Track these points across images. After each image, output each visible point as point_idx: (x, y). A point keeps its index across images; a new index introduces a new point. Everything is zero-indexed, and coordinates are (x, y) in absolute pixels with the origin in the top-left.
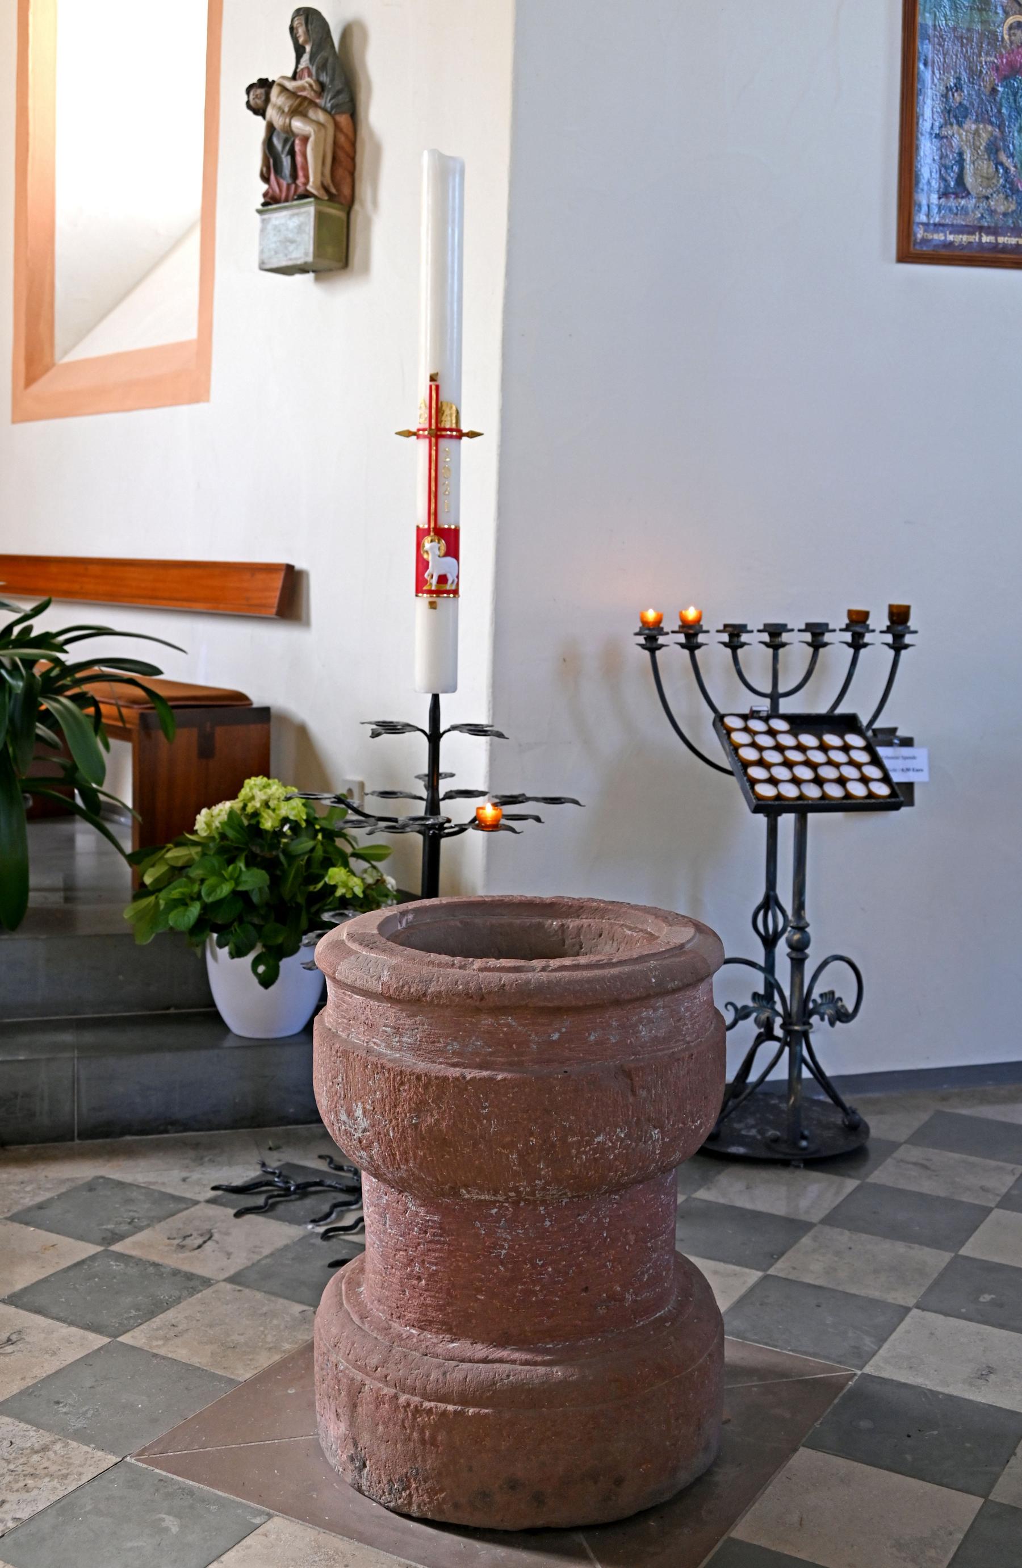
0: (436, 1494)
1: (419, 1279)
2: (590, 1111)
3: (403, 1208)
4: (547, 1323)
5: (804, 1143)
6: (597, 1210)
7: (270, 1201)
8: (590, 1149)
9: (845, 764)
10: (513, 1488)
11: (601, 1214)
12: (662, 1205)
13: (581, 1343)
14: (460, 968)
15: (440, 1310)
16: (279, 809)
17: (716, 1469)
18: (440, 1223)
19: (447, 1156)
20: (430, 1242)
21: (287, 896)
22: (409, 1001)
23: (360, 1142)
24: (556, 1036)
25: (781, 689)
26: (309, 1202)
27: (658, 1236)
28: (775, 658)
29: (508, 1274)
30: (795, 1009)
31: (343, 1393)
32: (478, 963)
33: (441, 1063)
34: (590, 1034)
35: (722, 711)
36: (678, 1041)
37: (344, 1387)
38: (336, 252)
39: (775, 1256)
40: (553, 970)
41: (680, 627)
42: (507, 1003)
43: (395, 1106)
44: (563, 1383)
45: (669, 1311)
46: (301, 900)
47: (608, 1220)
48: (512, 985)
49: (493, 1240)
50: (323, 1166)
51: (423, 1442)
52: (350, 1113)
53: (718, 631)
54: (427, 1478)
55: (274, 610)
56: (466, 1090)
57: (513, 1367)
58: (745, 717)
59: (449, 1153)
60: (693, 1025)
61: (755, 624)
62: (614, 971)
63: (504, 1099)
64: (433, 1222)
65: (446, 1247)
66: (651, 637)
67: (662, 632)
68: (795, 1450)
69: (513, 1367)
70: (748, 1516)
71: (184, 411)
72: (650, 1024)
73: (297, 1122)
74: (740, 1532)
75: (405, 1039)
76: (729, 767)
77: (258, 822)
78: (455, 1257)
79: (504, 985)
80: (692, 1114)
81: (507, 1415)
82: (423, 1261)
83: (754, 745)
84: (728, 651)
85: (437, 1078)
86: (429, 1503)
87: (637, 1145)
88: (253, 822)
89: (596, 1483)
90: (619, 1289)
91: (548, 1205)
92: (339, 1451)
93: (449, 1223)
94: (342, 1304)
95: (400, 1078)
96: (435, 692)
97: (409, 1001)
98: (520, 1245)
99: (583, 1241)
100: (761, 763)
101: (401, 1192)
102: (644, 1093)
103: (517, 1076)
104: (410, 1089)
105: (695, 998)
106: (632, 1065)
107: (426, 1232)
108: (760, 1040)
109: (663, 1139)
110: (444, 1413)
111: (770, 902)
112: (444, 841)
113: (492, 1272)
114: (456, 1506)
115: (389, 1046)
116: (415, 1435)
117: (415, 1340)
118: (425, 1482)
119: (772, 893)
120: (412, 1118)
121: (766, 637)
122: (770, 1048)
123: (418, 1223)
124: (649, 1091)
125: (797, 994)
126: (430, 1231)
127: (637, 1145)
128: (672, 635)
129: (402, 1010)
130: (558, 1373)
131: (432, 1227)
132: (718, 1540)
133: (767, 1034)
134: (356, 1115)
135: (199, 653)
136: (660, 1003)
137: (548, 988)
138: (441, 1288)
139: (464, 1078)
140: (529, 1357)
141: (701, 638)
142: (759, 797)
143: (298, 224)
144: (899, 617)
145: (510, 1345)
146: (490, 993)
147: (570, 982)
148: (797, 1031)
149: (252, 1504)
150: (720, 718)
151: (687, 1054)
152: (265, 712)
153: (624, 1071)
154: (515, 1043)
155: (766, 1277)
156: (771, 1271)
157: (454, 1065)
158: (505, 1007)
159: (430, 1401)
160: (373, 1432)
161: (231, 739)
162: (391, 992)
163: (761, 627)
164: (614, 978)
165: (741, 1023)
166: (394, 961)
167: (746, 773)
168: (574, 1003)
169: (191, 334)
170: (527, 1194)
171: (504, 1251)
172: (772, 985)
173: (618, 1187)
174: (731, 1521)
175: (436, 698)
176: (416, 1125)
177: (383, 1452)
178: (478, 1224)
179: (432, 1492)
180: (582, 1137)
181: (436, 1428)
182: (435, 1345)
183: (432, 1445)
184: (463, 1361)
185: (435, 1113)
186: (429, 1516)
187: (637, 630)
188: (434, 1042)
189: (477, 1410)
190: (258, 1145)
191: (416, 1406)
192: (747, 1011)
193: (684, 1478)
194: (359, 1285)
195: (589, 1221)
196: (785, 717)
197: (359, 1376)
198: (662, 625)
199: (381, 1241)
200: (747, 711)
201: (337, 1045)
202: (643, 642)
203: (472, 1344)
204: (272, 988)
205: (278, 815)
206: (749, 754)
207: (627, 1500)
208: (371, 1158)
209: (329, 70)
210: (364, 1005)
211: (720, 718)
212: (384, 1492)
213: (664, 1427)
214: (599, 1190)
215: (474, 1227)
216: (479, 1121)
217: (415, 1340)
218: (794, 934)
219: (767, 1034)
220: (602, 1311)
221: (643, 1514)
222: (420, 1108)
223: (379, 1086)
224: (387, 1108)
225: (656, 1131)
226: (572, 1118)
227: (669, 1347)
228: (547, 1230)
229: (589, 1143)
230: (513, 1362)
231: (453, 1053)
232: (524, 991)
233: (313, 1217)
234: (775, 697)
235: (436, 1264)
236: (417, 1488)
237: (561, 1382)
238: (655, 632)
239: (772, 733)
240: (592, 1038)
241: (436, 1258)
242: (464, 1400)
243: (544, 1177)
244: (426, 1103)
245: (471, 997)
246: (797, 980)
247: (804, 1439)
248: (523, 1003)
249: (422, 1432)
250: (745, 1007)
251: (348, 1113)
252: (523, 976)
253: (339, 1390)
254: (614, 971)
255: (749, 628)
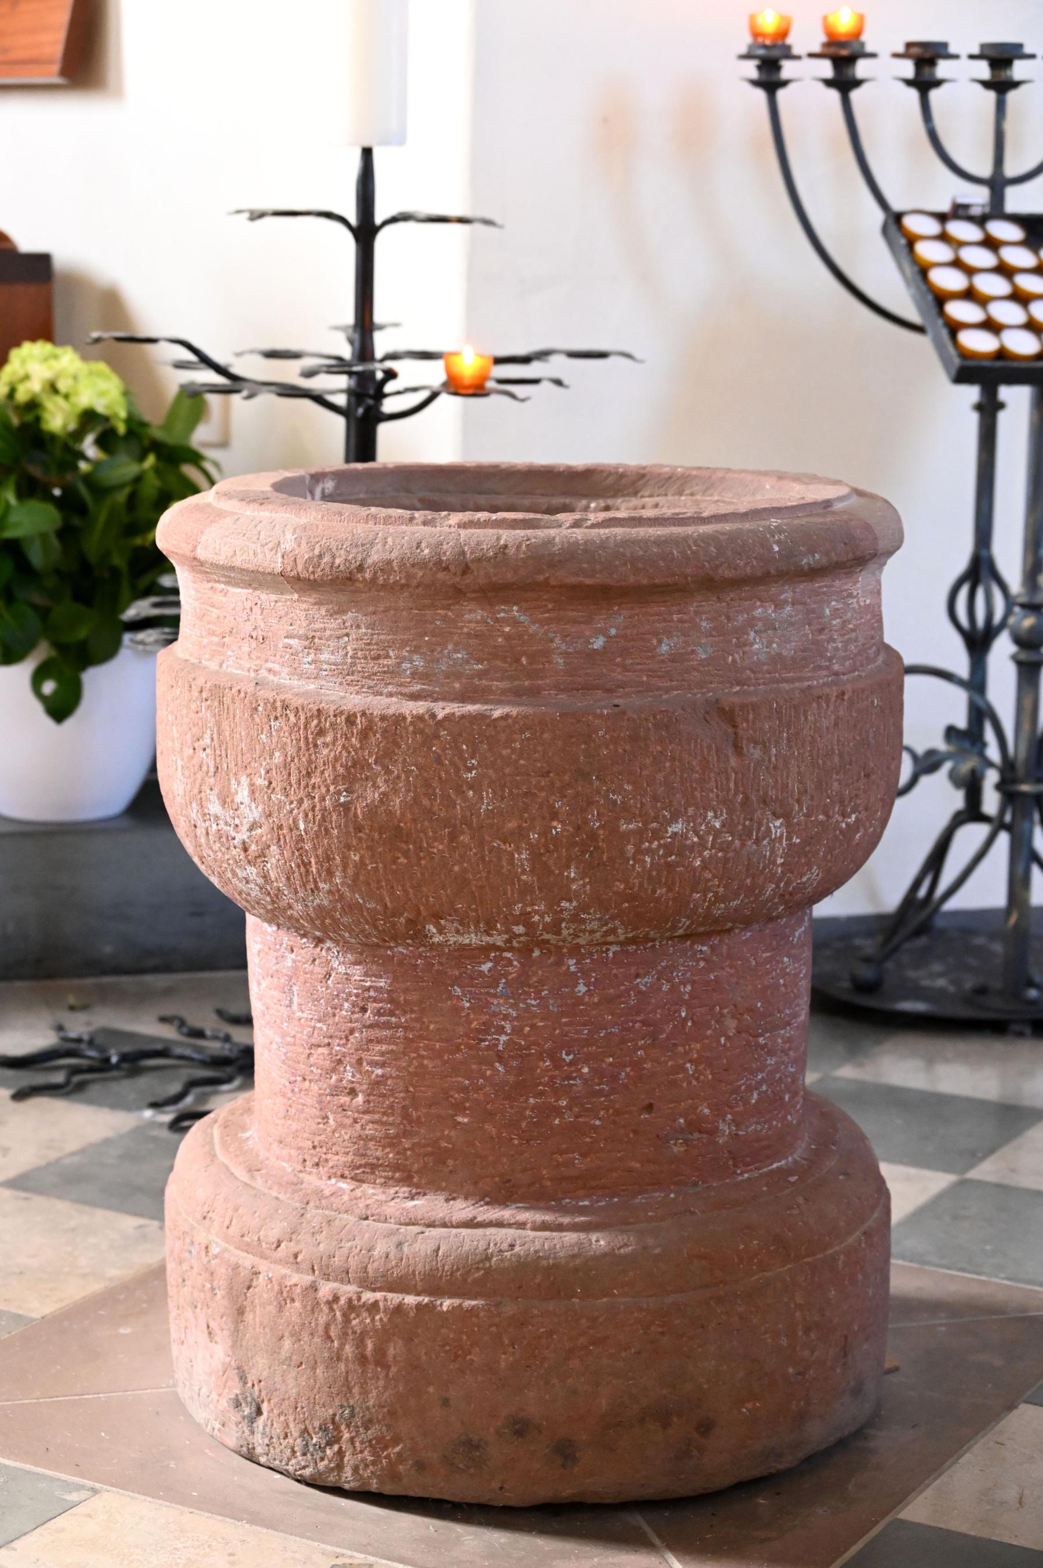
0: (386, 1448)
1: (353, 1092)
2: (660, 777)
3: (324, 971)
4: (580, 1163)
5: (1033, 993)
6: (672, 968)
7: (76, 1079)
8: (660, 846)
10: (519, 1433)
11: (677, 976)
12: (784, 974)
13: (640, 1199)
14: (425, 523)
15: (391, 1145)
16: (76, 394)
17: (872, 1432)
18: (389, 992)
19: (402, 860)
20: (371, 1026)
21: (93, 557)
22: (335, 584)
23: (245, 850)
24: (599, 643)
25: (1011, 170)
26: (143, 1082)
27: (775, 1028)
28: (1001, 108)
29: (511, 1079)
30: (1022, 754)
31: (220, 1294)
32: (456, 518)
33: (390, 695)
34: (660, 642)
35: (897, 205)
36: (820, 668)
37: (221, 1282)
39: (976, 1156)
40: (593, 526)
41: (826, 45)
42: (510, 577)
43: (309, 775)
44: (609, 1256)
45: (795, 1162)
46: (119, 561)
47: (689, 988)
48: (519, 547)
49: (484, 1018)
50: (168, 1033)
51: (362, 1359)
52: (226, 800)
53: (896, 56)
54: (370, 1421)
55: (56, 68)
56: (437, 737)
57: (518, 1233)
58: (942, 218)
59: (406, 854)
60: (847, 643)
61: (964, 41)
62: (703, 529)
63: (505, 752)
64: (377, 989)
65: (400, 1033)
66: (769, 66)
67: (788, 54)
68: (1011, 1407)
69: (518, 1233)
70: (929, 1493)
72: (770, 630)
73: (118, 970)
74: (918, 1510)
75: (325, 656)
76: (913, 315)
77: (38, 419)
78: (416, 1050)
79: (506, 546)
80: (842, 802)
81: (509, 1309)
82: (360, 1061)
83: (957, 263)
84: (913, 94)
85: (383, 718)
86: (374, 1463)
87: (743, 845)
88: (29, 418)
89: (666, 1426)
90: (706, 1111)
91: (583, 957)
92: (214, 1396)
93: (406, 991)
94: (214, 1156)
95: (316, 724)
96: (367, 144)
97: (335, 584)
98: (533, 1027)
99: (644, 1023)
100: (970, 295)
101: (319, 941)
102: (757, 753)
103: (530, 710)
104: (335, 740)
105: (851, 596)
106: (736, 700)
107: (364, 1010)
108: (959, 820)
109: (789, 838)
110: (399, 1309)
111: (980, 570)
112: (384, 430)
113: (483, 1075)
114: (421, 1466)
115: (296, 672)
116: (348, 1349)
117: (346, 1198)
118: (367, 1429)
119: (984, 553)
120: (339, 793)
121: (983, 70)
122: (973, 834)
123: (350, 994)
124: (766, 749)
125: (1026, 727)
126: (371, 1006)
127: (743, 845)
128: (808, 62)
129: (319, 603)
130: (599, 1242)
131: (375, 1000)
132: (876, 1523)
133: (972, 812)
134: (238, 799)
136: (787, 595)
137: (585, 551)
138: (391, 1107)
139: (433, 716)
140: (548, 1217)
141: (862, 68)
142: (965, 354)
145: (515, 1202)
146: (479, 560)
147: (626, 543)
148: (1024, 795)
149: (63, 1476)
150: (895, 219)
151: (834, 691)
152: (41, 263)
153: (721, 711)
154: (524, 653)
155: (962, 1183)
156: (973, 1174)
157: (414, 697)
158: (506, 587)
159: (374, 1290)
160: (274, 1352)
162: (300, 568)
163: (976, 51)
164: (705, 539)
165: (925, 781)
166: (303, 520)
167: (941, 312)
168: (632, 579)
170: (547, 929)
171: (503, 1038)
172: (981, 712)
173: (712, 928)
174: (901, 1498)
175: (367, 153)
176: (346, 807)
177: (292, 1384)
178: (458, 991)
179: (378, 1445)
180: (646, 823)
181: (384, 1336)
182: (381, 1203)
183: (377, 1363)
184: (431, 1225)
185: (380, 781)
186: (374, 1486)
187: (743, 50)
188: (377, 658)
189: (456, 1302)
190: (51, 1002)
191: (350, 1300)
192: (934, 759)
193: (817, 1433)
194: (244, 1128)
195: (655, 988)
196: (1017, 219)
197: (248, 1261)
198: (789, 41)
199: (284, 1035)
200: (945, 207)
201: (201, 681)
202: (754, 74)
203: (447, 1200)
204: (70, 723)
205: (74, 405)
206: (949, 280)
207: (718, 1462)
208: (265, 877)
210: (248, 604)
211: (895, 219)
212: (294, 1452)
213: (784, 1342)
214: (674, 928)
215: (450, 997)
216: (460, 792)
217: (346, 1198)
218: (1025, 617)
219: (972, 812)
220: (677, 1149)
221: (746, 1487)
222: (353, 773)
223: (279, 741)
224: (294, 779)
225: (778, 823)
226: (628, 787)
227: (796, 1212)
228: (579, 1001)
229: (657, 835)
230: (521, 1225)
231: (414, 675)
232: (543, 558)
233: (152, 1099)
234: (997, 184)
235: (383, 1065)
236: (352, 1440)
237: (605, 1255)
238: (775, 53)
239: (991, 244)
240: (664, 648)
241: (382, 1054)
242: (435, 1283)
243: (577, 896)
244: (365, 765)
245: (446, 569)
246: (1028, 703)
247: (1028, 1393)
248: (541, 578)
249: (360, 1342)
250: (931, 753)
252: (541, 534)
253: (213, 1289)
254: (703, 529)
255: (952, 49)
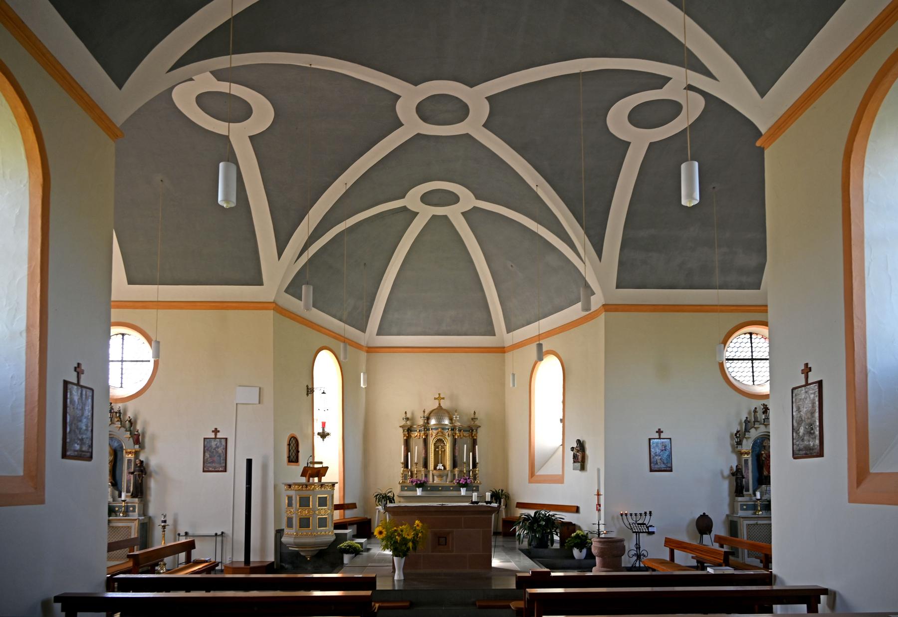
9: (644, 529)
38: (583, 468)
71: (560, 485)
72: (619, 544)
135: (567, 517)
143: (578, 465)
144: (650, 513)
161: (571, 528)
169: (561, 473)
209: (581, 446)
251: (594, 551)
